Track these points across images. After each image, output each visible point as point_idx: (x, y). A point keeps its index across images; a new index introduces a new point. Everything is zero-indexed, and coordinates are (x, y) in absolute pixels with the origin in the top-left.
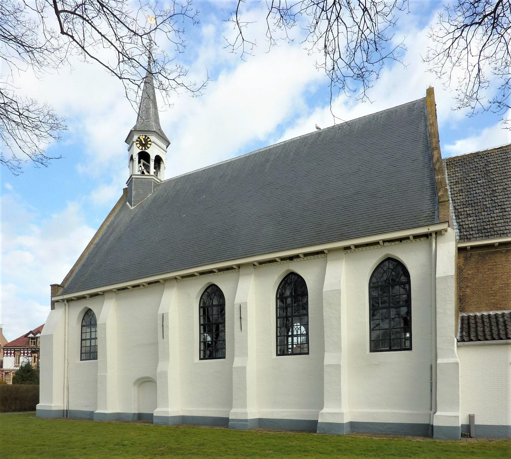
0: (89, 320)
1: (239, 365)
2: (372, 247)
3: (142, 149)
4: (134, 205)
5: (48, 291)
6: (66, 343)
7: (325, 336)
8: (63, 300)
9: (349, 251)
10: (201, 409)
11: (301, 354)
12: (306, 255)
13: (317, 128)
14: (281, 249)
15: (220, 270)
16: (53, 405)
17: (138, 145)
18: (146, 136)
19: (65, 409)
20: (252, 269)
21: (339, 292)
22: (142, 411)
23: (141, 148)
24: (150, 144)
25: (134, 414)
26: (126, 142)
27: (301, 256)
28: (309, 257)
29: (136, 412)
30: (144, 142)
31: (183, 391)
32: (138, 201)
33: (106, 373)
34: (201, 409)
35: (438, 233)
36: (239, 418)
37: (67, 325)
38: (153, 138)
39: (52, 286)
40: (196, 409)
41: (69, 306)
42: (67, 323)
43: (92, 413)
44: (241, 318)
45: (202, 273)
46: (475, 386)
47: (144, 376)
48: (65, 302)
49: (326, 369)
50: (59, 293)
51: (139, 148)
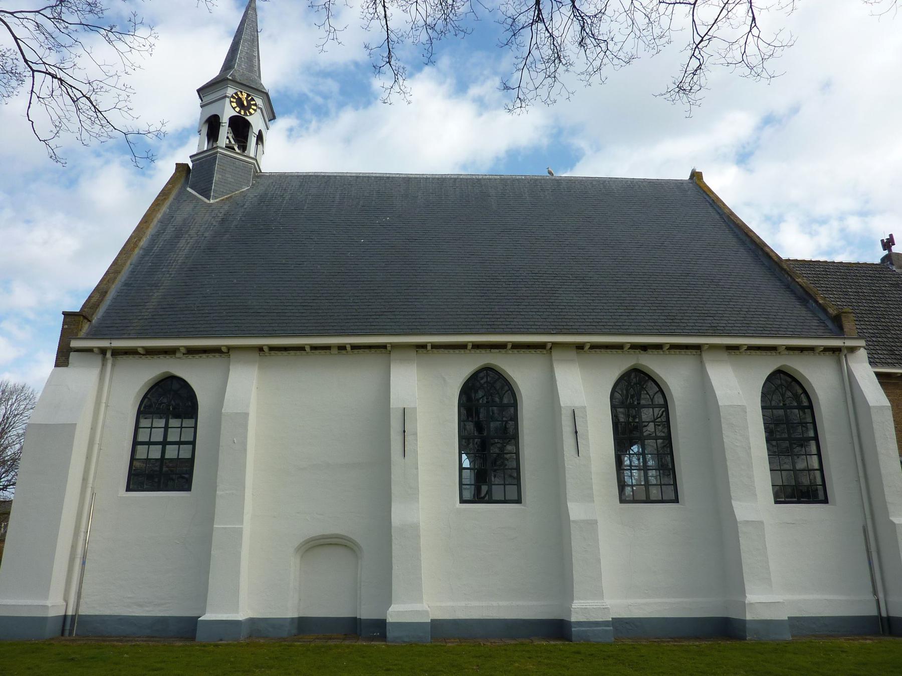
0: (170, 401)
1: (583, 517)
2: (764, 353)
3: (239, 112)
4: (215, 198)
5: (58, 323)
6: (96, 447)
7: (730, 475)
8: (103, 351)
9: (344, 352)
10: (476, 603)
11: (662, 501)
12: (751, 348)
13: (550, 173)
14: (565, 331)
15: (517, 346)
16: (49, 603)
17: (234, 105)
18: (248, 95)
19: (70, 612)
20: (256, 355)
21: (246, 415)
22: (302, 615)
23: (238, 109)
24: (255, 110)
25: (293, 619)
26: (199, 91)
27: (266, 349)
28: (317, 352)
29: (296, 616)
30: (245, 103)
31: (446, 567)
32: (223, 194)
33: (242, 522)
34: (476, 603)
35: (852, 350)
36: (591, 620)
37: (103, 406)
38: (259, 101)
39: (64, 313)
40: (463, 604)
41: (113, 365)
42: (104, 400)
43: (193, 622)
44: (576, 432)
45: (477, 346)
46: (789, 569)
47: (328, 532)
48: (109, 355)
49: (742, 529)
50: (82, 334)
51: (234, 108)
